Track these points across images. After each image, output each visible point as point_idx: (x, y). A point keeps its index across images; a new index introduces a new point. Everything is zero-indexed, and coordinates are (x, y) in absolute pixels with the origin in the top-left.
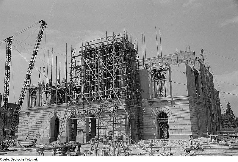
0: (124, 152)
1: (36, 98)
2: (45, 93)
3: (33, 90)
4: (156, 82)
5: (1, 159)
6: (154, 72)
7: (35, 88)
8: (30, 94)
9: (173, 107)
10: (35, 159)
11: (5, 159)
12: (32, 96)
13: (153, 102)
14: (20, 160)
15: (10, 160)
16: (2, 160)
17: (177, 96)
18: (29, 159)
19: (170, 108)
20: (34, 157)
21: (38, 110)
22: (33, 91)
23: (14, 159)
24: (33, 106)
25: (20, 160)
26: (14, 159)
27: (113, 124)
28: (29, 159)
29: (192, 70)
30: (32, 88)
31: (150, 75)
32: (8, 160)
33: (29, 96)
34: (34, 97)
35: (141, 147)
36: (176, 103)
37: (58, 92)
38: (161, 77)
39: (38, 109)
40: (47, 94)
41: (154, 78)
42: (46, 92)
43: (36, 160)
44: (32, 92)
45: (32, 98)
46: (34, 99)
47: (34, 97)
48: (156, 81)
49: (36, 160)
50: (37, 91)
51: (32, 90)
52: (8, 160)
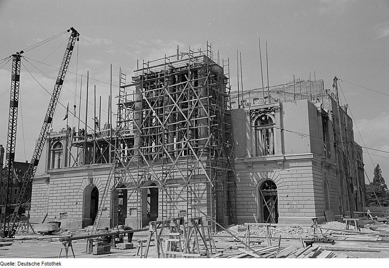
1: (60, 153)
2: (76, 146)
5: (2, 264)
6: (256, 114)
7: (59, 137)
10: (57, 263)
11: (8, 263)
13: (253, 163)
14: (33, 264)
15: (16, 264)
17: (292, 154)
18: (47, 264)
19: (280, 173)
20: (56, 260)
21: (63, 174)
22: (56, 142)
24: (56, 167)
25: (33, 264)
26: (22, 264)
28: (47, 264)
29: (318, 111)
31: (248, 118)
32: (13, 264)
33: (50, 151)
36: (291, 165)
38: (267, 121)
39: (63, 173)
41: (256, 124)
44: (54, 144)
45: (54, 153)
46: (58, 156)
48: (258, 128)
50: (63, 142)
51: (54, 141)
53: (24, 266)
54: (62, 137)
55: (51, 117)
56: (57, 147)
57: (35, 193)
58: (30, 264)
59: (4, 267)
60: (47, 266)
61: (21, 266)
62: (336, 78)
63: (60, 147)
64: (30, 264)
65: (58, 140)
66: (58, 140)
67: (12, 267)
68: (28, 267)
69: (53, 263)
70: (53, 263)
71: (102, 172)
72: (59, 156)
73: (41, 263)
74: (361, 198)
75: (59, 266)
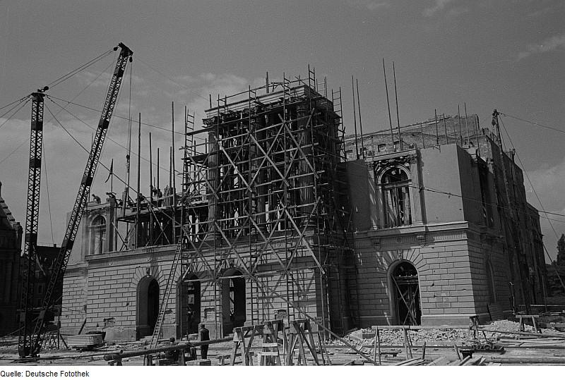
4: (387, 189)
5: (3, 373)
9: (428, 249)
10: (83, 373)
11: (12, 373)
14: (48, 374)
15: (24, 374)
16: (5, 375)
18: (69, 374)
23: (32, 374)
25: (48, 374)
26: (32, 374)
27: (283, 295)
29: (472, 160)
31: (372, 173)
32: (18, 374)
36: (437, 239)
40: (128, 222)
41: (383, 180)
42: (127, 219)
43: (85, 374)
48: (386, 187)
49: (85, 374)
52: (18, 374)
54: (104, 208)
57: (67, 298)
58: (43, 374)
62: (496, 112)
64: (43, 374)
69: (77, 374)
70: (77, 374)
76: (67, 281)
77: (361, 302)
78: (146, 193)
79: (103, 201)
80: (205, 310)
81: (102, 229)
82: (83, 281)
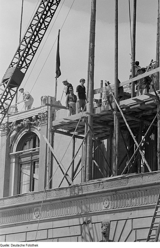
0: (125, 220)
1: (33, 164)
2: (68, 134)
3: (23, 127)
5: (1, 245)
7: (30, 119)
8: (9, 148)
10: (36, 245)
11: (5, 245)
12: (18, 157)
14: (20, 246)
15: (10, 246)
18: (29, 245)
20: (35, 243)
21: (30, 211)
22: (24, 133)
23: (14, 245)
24: (25, 189)
25: (20, 246)
26: (14, 245)
28: (29, 245)
30: (18, 122)
32: (8, 246)
33: (8, 157)
34: (26, 163)
35: (82, 169)
37: (122, 127)
39: (28, 209)
40: (75, 137)
42: (70, 129)
44: (19, 138)
45: (20, 165)
46: (29, 172)
47: (26, 163)
50: (41, 131)
51: (19, 130)
52: (8, 246)
53: (15, 247)
54: (37, 117)
55: (23, 70)
56: (27, 146)
58: (19, 246)
59: (2, 247)
60: (29, 247)
61: (13, 247)
63: (34, 147)
64: (19, 246)
65: (30, 126)
66: (30, 126)
67: (7, 247)
68: (18, 247)
69: (33, 245)
70: (33, 245)
71: (134, 201)
72: (33, 171)
73: (25, 245)
74: (98, 175)
75: (37, 247)
76: (159, 181)
77: (100, 202)
78: (125, 78)
79: (37, 103)
80: (54, 195)
81: (34, 157)
82: (157, 182)
